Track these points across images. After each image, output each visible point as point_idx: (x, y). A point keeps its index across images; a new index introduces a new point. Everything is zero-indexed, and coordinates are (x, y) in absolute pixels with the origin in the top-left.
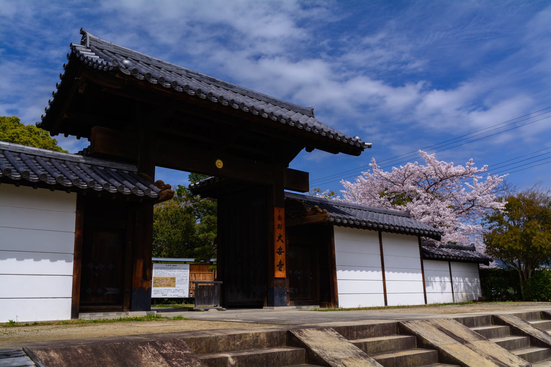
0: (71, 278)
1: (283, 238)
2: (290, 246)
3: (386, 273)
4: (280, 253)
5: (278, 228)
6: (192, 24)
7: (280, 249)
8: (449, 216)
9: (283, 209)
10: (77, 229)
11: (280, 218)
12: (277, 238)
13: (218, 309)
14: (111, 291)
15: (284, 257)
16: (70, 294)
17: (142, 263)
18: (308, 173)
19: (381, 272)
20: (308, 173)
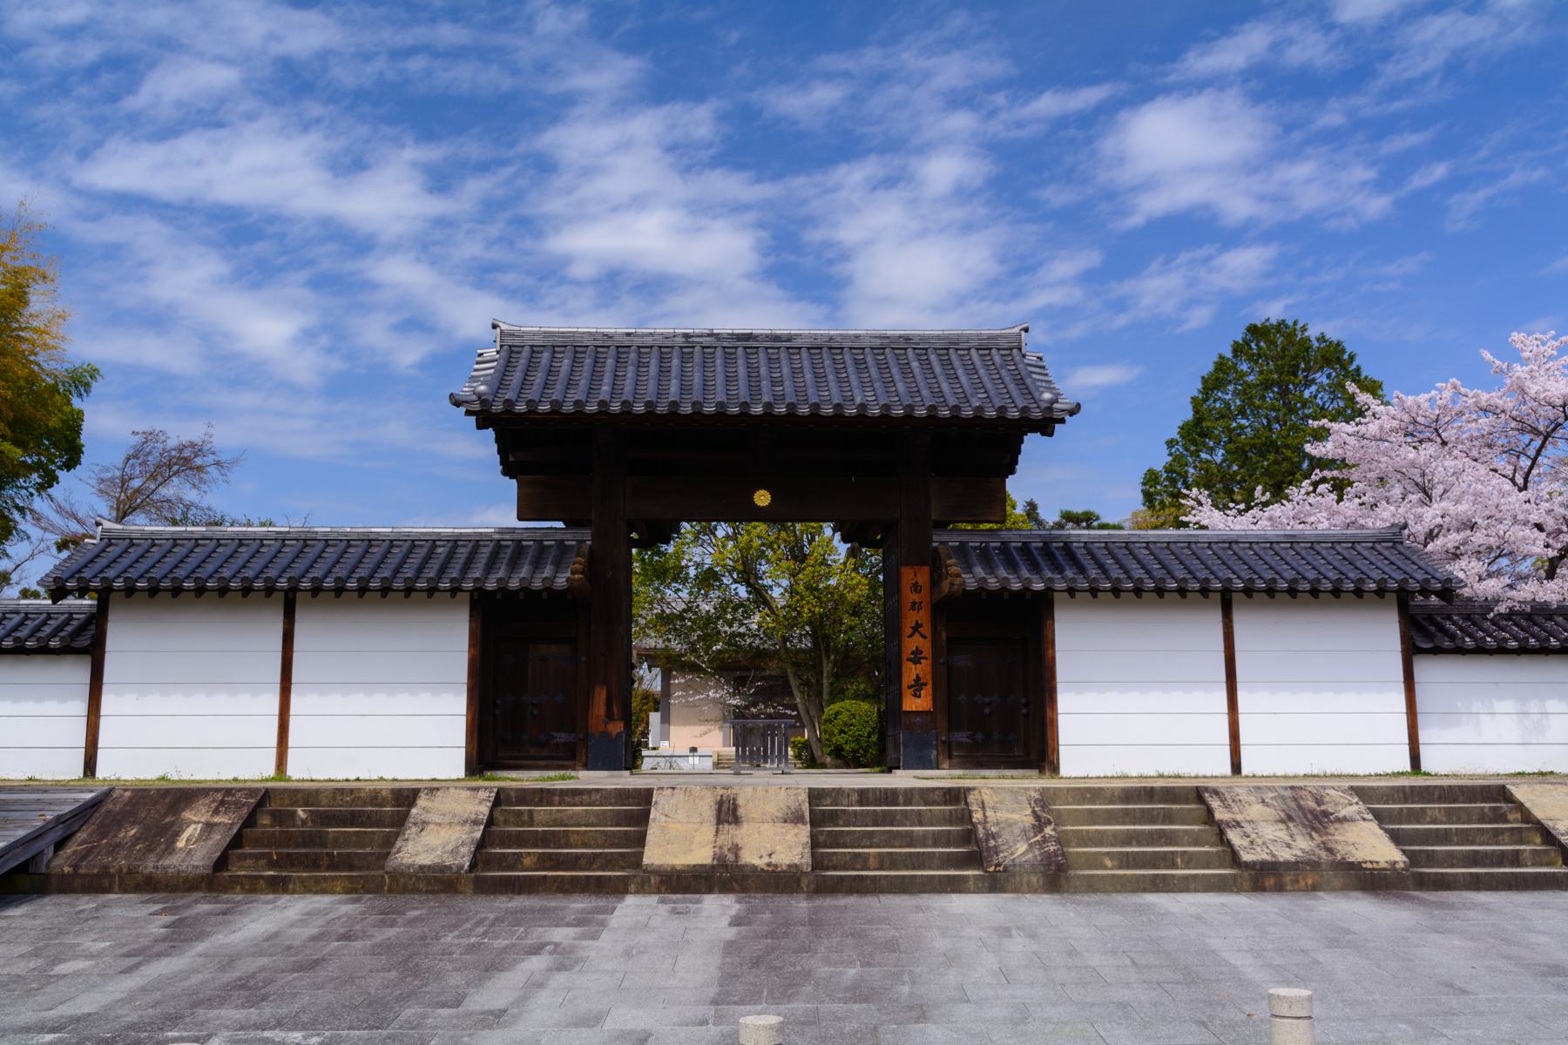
0: (464, 719)
1: (926, 629)
2: (943, 653)
3: (108, 702)
4: (916, 661)
5: (913, 608)
6: (921, 1007)
7: (917, 652)
8: (107, 860)
9: (926, 569)
10: (471, 645)
11: (916, 588)
12: (908, 631)
13: (1087, 519)
14: (562, 737)
15: (929, 669)
16: (463, 743)
17: (603, 695)
18: (1051, 435)
19: (80, 707)
20: (1051, 435)
